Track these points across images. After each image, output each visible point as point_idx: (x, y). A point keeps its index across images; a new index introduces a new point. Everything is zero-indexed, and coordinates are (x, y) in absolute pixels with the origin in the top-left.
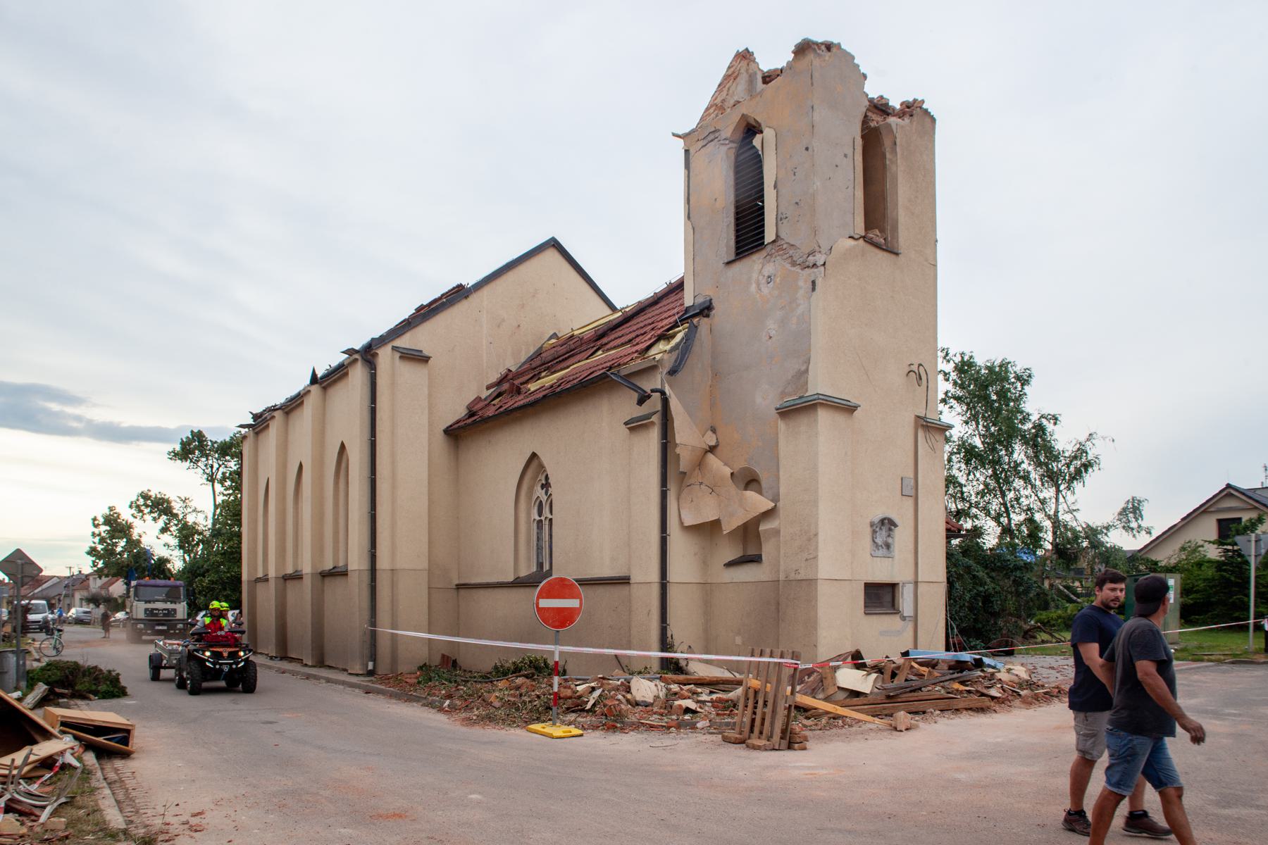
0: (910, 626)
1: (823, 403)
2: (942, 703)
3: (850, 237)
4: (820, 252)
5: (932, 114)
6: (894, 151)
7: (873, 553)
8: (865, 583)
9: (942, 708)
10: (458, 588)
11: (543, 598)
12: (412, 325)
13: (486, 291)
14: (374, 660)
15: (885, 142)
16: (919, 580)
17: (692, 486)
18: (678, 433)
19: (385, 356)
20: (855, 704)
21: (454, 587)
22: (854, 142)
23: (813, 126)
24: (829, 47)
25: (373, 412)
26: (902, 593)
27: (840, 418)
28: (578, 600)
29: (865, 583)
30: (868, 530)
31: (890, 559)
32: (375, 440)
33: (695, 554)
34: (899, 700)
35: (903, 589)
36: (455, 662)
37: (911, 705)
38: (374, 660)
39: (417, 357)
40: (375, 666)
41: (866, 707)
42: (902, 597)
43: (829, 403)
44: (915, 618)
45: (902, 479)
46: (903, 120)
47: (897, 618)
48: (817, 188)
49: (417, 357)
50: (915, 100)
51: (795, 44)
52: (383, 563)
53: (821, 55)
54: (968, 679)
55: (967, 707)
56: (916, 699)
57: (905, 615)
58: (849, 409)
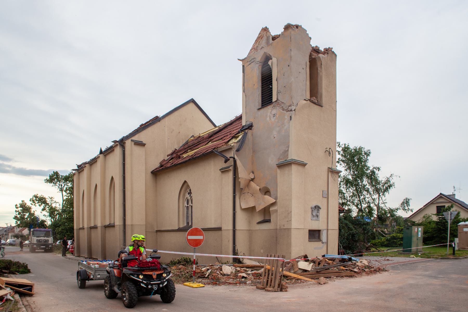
0: (325, 246)
2: (337, 274)
3: (304, 100)
5: (335, 53)
6: (321, 67)
8: (309, 230)
9: (337, 276)
11: (189, 236)
12: (139, 132)
13: (167, 119)
17: (245, 193)
19: (128, 143)
21: (155, 231)
24: (297, 26)
26: (322, 233)
27: (300, 168)
28: (203, 236)
29: (309, 230)
30: (310, 210)
31: (318, 221)
32: (125, 176)
33: (246, 219)
34: (321, 273)
39: (140, 144)
42: (322, 235)
44: (327, 243)
47: (320, 243)
49: (140, 144)
50: (329, 48)
53: (294, 30)
55: (346, 275)
56: (327, 272)
58: (304, 165)
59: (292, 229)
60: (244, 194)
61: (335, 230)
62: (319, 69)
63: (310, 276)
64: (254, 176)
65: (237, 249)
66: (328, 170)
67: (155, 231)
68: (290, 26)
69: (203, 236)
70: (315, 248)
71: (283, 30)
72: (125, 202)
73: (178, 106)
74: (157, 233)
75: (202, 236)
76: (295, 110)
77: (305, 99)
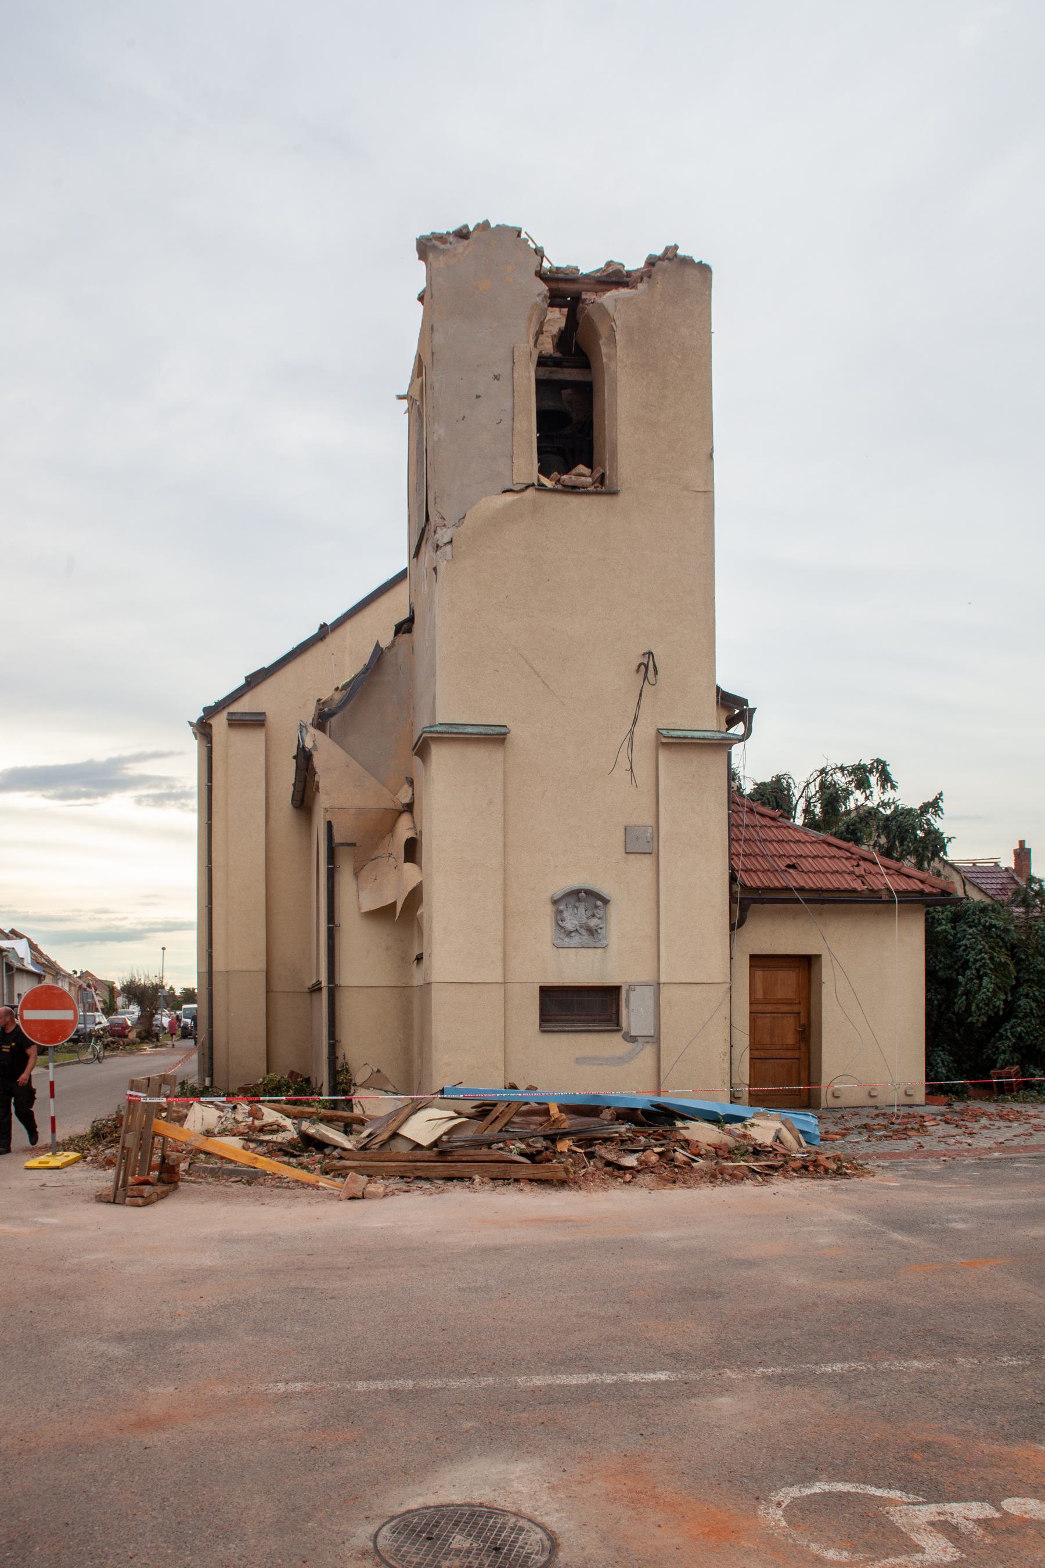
1: (434, 737)
3: (504, 492)
4: (445, 526)
7: (557, 942)
8: (541, 987)
9: (495, 1175)
10: (311, 992)
12: (253, 685)
14: (211, 1076)
15: (601, 332)
16: (662, 980)
17: (379, 859)
18: (288, 802)
19: (219, 723)
20: (418, 1158)
21: (307, 990)
22: (513, 353)
23: (433, 353)
24: (462, 234)
25: (210, 789)
26: (627, 1000)
27: (480, 756)
28: (72, 1011)
29: (541, 987)
30: (549, 909)
31: (600, 951)
32: (211, 824)
33: (387, 949)
34: (450, 1158)
35: (628, 995)
36: (308, 1081)
37: (452, 1167)
38: (211, 1076)
39: (255, 722)
40: (212, 1082)
41: (393, 1164)
42: (627, 1006)
43: (473, 736)
44: (655, 1039)
45: (625, 829)
46: (636, 289)
47: (617, 1038)
48: (439, 439)
49: (255, 722)
50: (667, 249)
51: (422, 234)
52: (218, 965)
54: (599, 1135)
55: (531, 1177)
56: (469, 1158)
57: (633, 1033)
59: (433, 986)
60: (374, 861)
61: (700, 987)
62: (604, 350)
63: (395, 1166)
64: (413, 794)
65: (344, 1055)
66: (657, 738)
67: (307, 990)
68: (426, 246)
69: (72, 1011)
70: (579, 1061)
71: (422, 263)
72: (211, 905)
73: (390, 578)
74: (311, 995)
75: (71, 1009)
76: (451, 542)
77: (509, 486)
